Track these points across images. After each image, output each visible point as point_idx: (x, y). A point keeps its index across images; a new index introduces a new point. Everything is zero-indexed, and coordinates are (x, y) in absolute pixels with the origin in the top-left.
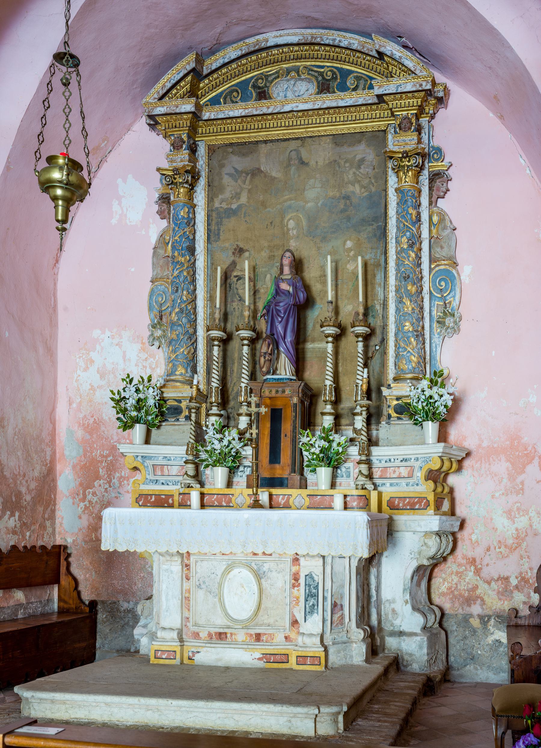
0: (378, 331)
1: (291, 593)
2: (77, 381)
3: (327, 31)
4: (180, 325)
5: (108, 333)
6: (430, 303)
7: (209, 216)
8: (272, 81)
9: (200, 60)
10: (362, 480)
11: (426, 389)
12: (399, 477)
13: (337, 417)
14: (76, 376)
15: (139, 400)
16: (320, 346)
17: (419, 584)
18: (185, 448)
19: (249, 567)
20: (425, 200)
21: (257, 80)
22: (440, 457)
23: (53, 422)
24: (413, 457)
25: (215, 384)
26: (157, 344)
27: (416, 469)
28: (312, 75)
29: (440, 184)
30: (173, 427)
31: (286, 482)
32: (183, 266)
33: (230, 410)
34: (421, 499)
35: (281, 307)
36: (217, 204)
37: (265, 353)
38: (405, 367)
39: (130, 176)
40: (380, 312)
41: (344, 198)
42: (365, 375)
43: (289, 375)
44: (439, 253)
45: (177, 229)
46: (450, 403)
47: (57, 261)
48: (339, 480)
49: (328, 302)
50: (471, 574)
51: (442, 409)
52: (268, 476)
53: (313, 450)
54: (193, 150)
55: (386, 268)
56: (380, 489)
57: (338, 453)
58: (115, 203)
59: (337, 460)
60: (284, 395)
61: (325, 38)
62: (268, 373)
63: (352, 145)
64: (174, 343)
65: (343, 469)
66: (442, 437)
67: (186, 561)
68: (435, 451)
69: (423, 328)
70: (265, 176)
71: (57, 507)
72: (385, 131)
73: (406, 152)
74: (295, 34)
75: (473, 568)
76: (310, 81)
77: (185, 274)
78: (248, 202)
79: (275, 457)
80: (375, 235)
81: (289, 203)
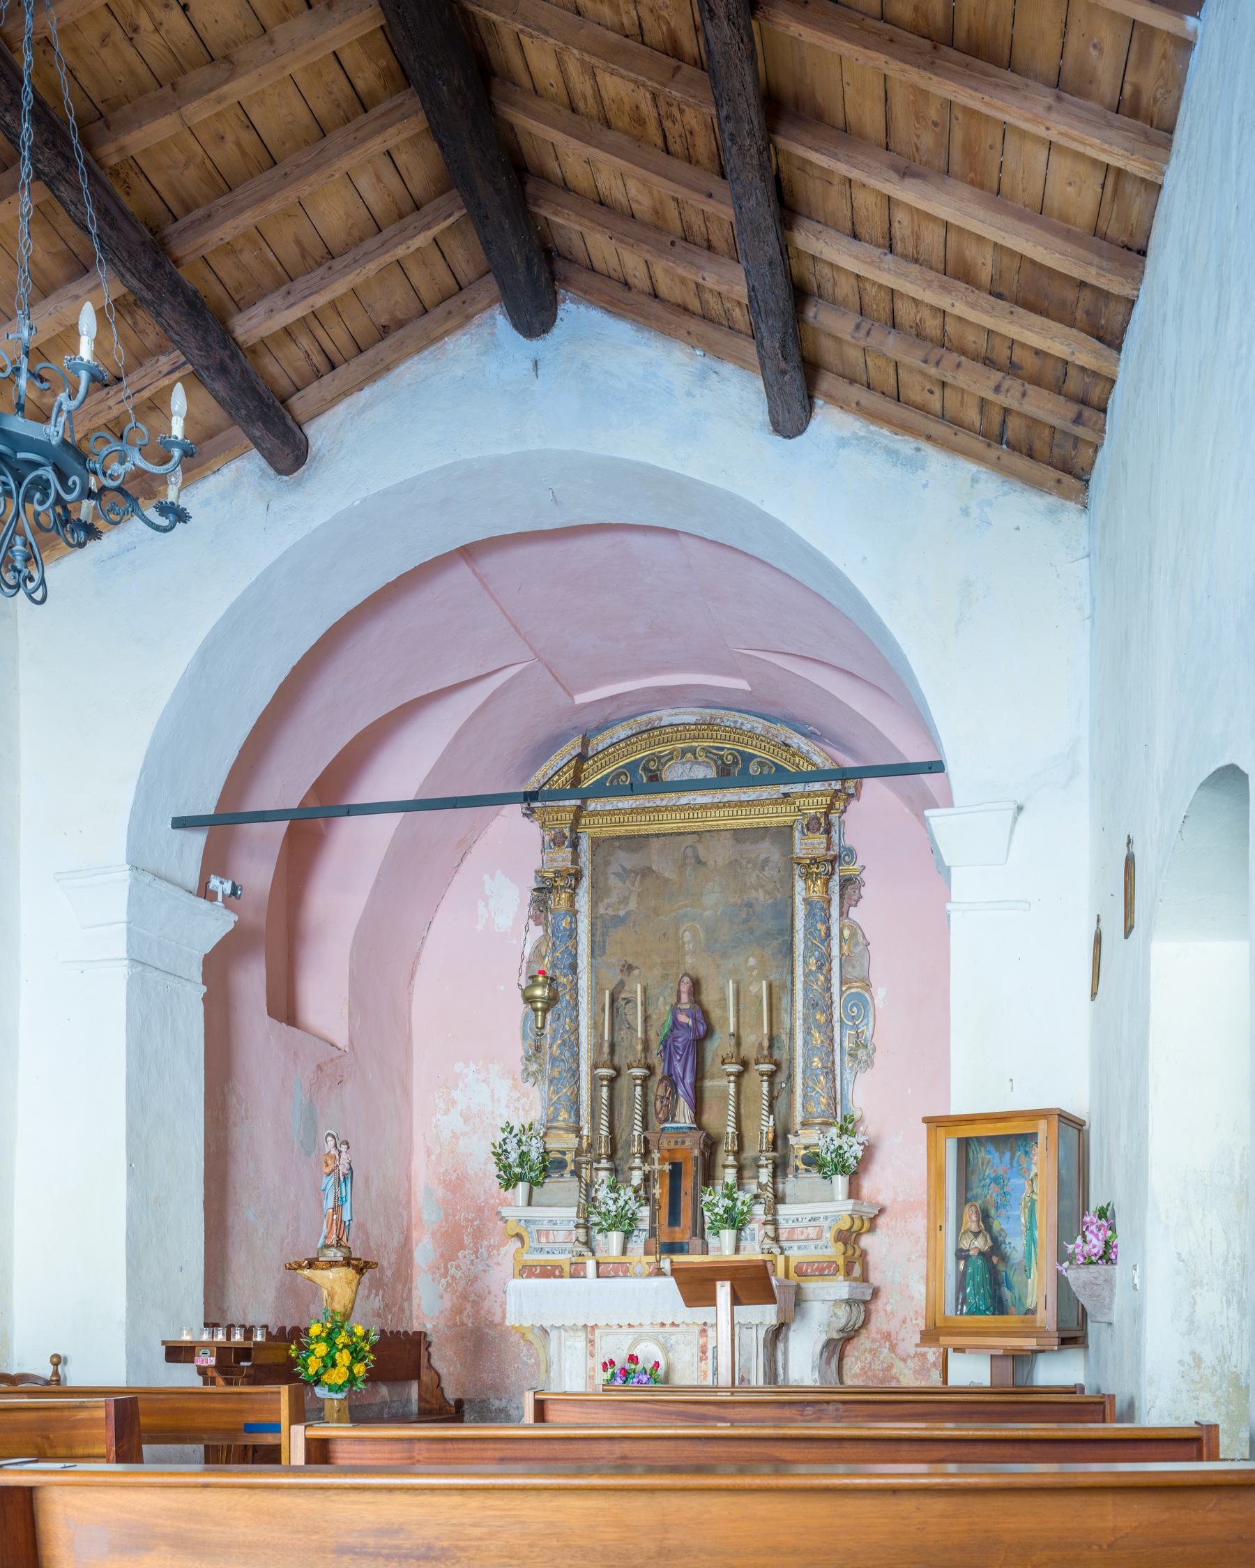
0: (784, 1066)
1: (699, 1367)
2: (436, 1126)
3: (727, 712)
4: (563, 1060)
5: (473, 1067)
6: (841, 1033)
7: (593, 925)
8: (666, 763)
9: (585, 744)
10: (768, 1243)
11: (835, 1138)
12: (807, 1239)
13: (740, 1169)
14: (434, 1121)
15: (523, 1153)
16: (719, 1083)
17: (828, 1362)
18: (575, 1209)
19: (655, 1340)
20: (835, 911)
21: (648, 761)
22: (850, 1215)
23: (409, 1179)
24: (822, 1216)
25: (604, 1132)
26: (532, 1080)
27: (825, 1229)
28: (711, 758)
29: (852, 891)
30: (558, 1184)
31: (686, 1247)
32: (566, 988)
33: (617, 1162)
34: (830, 1263)
35: (680, 1042)
36: (602, 911)
37: (663, 1097)
38: (814, 1109)
39: (499, 872)
40: (786, 1042)
41: (746, 905)
42: (771, 1123)
43: (688, 1124)
44: (851, 973)
45: (558, 943)
46: (860, 1155)
47: (412, 978)
48: (742, 1244)
49: (730, 1035)
50: (886, 1351)
51: (852, 1161)
52: (667, 1241)
53: (716, 1210)
54: (575, 845)
55: (792, 990)
56: (787, 1253)
57: (742, 1213)
58: (481, 905)
59: (741, 1221)
60: (684, 1147)
61: (725, 719)
62: (666, 1120)
63: (755, 841)
64: (555, 1081)
65: (748, 1231)
66: (854, 1192)
67: (590, 1336)
68: (844, 1208)
69: (833, 1062)
70: (657, 877)
71: (414, 1285)
72: (791, 827)
73: (814, 859)
74: (692, 714)
75: (887, 1344)
76: (708, 765)
77: (568, 997)
78: (638, 908)
79: (674, 1217)
80: (781, 952)
81: (684, 910)
